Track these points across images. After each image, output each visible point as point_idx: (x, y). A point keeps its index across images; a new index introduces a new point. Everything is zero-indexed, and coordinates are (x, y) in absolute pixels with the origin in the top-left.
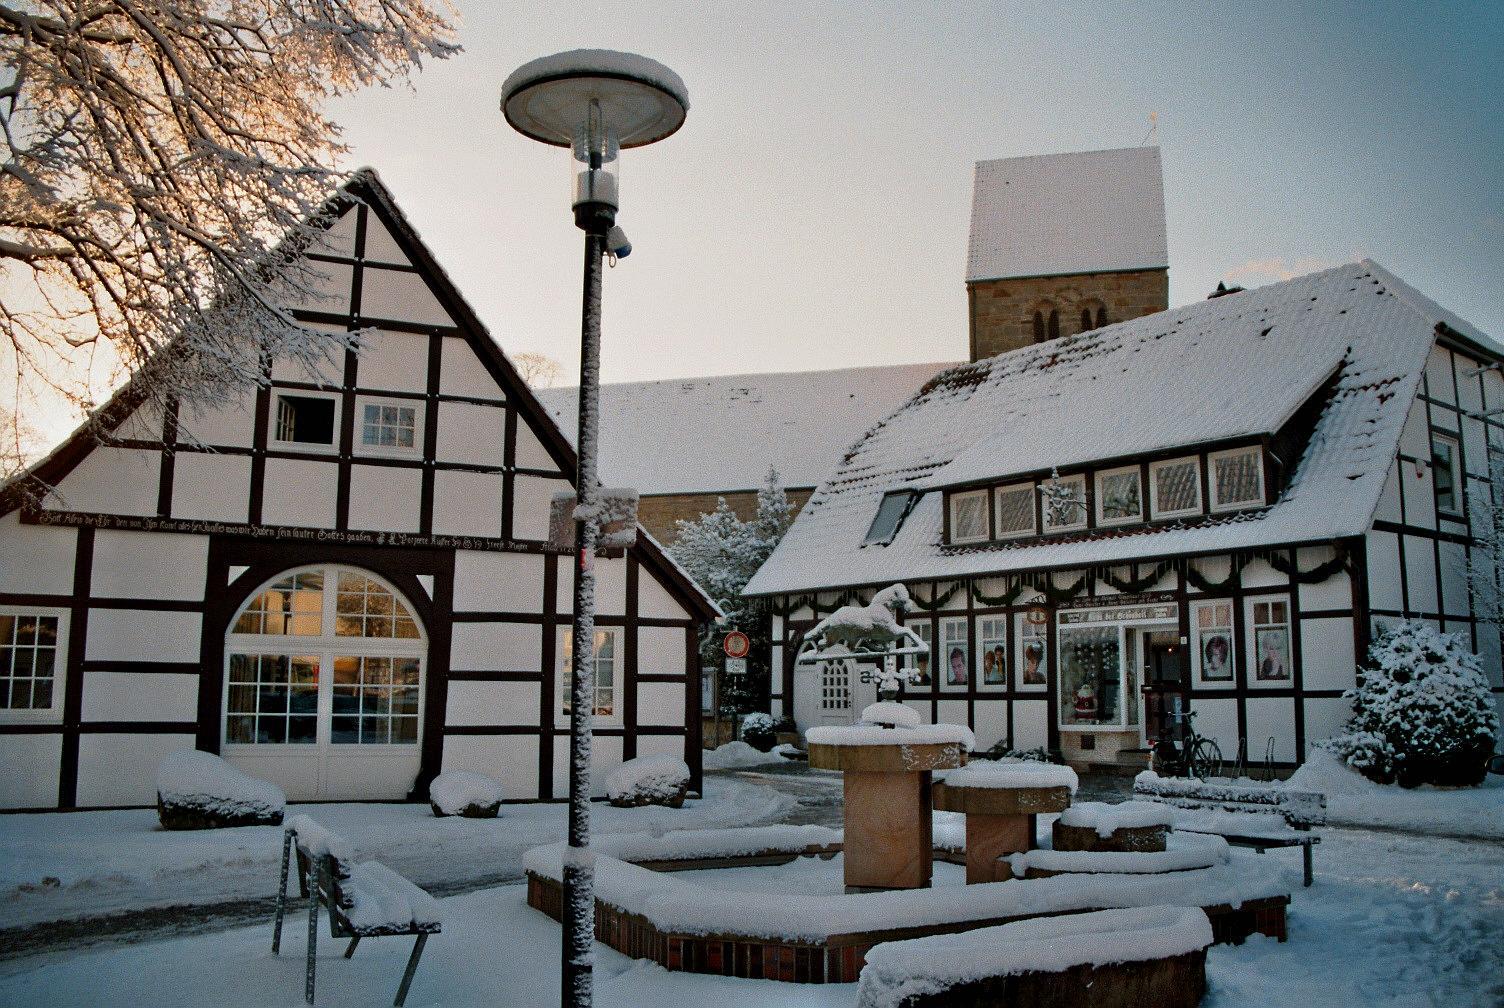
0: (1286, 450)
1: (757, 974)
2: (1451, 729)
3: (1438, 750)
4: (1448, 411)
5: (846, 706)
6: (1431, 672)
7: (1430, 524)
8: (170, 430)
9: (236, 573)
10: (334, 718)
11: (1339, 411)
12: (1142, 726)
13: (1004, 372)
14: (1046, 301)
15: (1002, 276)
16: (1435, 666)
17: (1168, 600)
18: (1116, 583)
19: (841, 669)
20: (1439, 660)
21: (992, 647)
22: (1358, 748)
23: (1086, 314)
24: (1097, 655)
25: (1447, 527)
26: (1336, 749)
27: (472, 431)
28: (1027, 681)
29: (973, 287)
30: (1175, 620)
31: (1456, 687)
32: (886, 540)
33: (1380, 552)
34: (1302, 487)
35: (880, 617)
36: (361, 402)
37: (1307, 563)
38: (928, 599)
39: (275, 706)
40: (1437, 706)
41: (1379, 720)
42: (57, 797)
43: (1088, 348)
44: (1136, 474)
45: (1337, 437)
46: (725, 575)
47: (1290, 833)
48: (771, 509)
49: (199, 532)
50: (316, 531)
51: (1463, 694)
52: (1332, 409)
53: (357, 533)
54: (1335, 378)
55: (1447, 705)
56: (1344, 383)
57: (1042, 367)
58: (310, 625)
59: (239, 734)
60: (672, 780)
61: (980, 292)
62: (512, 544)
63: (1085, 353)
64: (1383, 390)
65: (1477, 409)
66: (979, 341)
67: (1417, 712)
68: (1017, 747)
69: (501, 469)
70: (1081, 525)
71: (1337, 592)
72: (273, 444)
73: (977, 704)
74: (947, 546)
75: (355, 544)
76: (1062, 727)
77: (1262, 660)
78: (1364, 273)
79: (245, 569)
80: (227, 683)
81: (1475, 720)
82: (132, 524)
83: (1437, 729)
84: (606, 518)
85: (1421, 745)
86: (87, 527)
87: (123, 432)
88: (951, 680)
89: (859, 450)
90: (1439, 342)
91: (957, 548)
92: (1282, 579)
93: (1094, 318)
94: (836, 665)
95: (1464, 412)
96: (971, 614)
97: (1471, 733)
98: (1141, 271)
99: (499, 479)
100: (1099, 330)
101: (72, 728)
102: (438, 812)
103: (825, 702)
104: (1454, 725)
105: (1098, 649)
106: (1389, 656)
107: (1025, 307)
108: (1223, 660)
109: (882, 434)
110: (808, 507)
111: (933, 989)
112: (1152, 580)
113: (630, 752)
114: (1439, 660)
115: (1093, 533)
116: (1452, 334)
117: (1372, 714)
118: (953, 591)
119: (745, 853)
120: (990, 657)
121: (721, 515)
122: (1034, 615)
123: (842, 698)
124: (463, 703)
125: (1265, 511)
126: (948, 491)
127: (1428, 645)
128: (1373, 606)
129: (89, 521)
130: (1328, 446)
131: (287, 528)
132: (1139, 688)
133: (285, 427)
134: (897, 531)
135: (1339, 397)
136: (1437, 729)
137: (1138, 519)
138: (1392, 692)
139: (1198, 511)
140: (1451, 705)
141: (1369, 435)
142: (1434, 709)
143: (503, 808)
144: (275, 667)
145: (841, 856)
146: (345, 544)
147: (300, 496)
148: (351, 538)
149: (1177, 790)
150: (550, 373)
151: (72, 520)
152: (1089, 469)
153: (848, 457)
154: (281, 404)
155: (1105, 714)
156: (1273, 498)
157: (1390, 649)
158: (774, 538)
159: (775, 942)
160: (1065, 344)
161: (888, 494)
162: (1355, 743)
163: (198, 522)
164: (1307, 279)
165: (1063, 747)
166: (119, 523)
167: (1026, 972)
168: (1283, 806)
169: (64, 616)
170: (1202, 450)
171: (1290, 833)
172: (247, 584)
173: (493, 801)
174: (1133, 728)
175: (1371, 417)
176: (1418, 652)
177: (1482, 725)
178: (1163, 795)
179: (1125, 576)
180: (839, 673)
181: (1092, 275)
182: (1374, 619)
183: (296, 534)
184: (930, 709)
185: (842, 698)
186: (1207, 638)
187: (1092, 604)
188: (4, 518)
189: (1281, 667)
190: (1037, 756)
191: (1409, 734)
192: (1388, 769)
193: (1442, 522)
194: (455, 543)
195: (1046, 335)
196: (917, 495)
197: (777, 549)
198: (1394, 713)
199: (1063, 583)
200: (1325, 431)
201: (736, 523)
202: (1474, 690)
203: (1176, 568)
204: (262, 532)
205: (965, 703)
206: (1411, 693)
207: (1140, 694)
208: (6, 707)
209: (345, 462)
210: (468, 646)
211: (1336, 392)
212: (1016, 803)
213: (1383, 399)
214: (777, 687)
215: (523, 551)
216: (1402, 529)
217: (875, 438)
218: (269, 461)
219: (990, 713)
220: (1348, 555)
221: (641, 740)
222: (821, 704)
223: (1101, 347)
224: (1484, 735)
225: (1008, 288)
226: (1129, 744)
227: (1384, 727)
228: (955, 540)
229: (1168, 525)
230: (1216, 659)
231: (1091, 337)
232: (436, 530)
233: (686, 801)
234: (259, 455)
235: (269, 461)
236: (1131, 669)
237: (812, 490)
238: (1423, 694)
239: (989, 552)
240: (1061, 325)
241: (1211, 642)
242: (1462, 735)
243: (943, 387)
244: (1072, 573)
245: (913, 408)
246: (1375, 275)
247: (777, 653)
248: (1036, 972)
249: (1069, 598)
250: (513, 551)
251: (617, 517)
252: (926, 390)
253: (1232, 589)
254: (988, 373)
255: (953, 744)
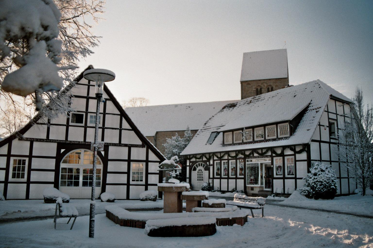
0: (295, 123)
1: (135, 227)
2: (325, 186)
3: (322, 191)
4: (334, 114)
5: (202, 180)
6: (322, 174)
7: (328, 140)
8: (49, 122)
9: (62, 150)
10: (83, 181)
11: (307, 115)
12: (264, 185)
13: (240, 105)
14: (259, 86)
15: (248, 80)
16: (323, 173)
17: (269, 157)
18: (258, 153)
19: (201, 172)
20: (324, 171)
21: (233, 167)
22: (304, 190)
23: (268, 89)
24: (254, 169)
25: (332, 141)
26: (300, 191)
27: (113, 121)
28: (240, 175)
29: (242, 83)
30: (270, 162)
31: (327, 177)
32: (211, 143)
33: (314, 147)
34: (297, 132)
35: (172, 162)
36: (89, 115)
37: (298, 149)
38: (219, 156)
39: (72, 179)
40: (322, 181)
41: (310, 185)
42: (25, 196)
43: (258, 99)
44: (251, 131)
45: (306, 121)
46: (176, 151)
47: (259, 207)
48: (187, 136)
49: (55, 142)
50: (79, 142)
51: (328, 179)
52: (306, 114)
53: (88, 142)
54: (308, 107)
55: (325, 181)
56: (309, 108)
57: (248, 103)
58: (84, 161)
59: (64, 184)
60: (153, 195)
61: (243, 84)
62: (121, 145)
63: (257, 100)
64: (317, 110)
65: (342, 113)
66: (243, 96)
67: (318, 183)
68: (238, 189)
69: (119, 129)
70: (251, 140)
71: (304, 156)
72: (70, 124)
73: (229, 180)
74: (224, 144)
75: (87, 145)
76: (247, 186)
77: (289, 171)
78: (317, 83)
79: (64, 150)
80: (60, 174)
81: (331, 184)
82: (41, 140)
83: (322, 186)
84: (99, 146)
85: (318, 190)
86: (32, 141)
87: (39, 121)
88: (224, 175)
89: (208, 122)
90: (331, 99)
91: (225, 145)
92: (292, 153)
93: (270, 90)
94: (200, 171)
95: (338, 115)
96: (228, 160)
97: (330, 187)
98: (281, 79)
99: (118, 131)
100: (261, 95)
101: (29, 182)
102: (102, 201)
103: (198, 179)
104: (326, 186)
105: (255, 168)
106: (313, 170)
107: (254, 87)
108: (280, 171)
109: (213, 118)
110: (196, 135)
111: (156, 228)
112: (265, 153)
113: (146, 189)
114: (324, 171)
115: (254, 142)
116: (334, 97)
117: (308, 183)
118: (224, 155)
119: (151, 208)
120: (232, 169)
121: (176, 137)
122: (240, 160)
123: (201, 178)
124: (110, 178)
125: (289, 137)
126: (224, 132)
127: (321, 168)
128: (312, 159)
129: (32, 140)
130: (304, 123)
131: (73, 141)
132: (264, 177)
133: (73, 120)
134: (214, 141)
135: (308, 111)
136: (322, 186)
137: (263, 139)
138: (313, 178)
139: (275, 137)
140: (325, 181)
141: (313, 120)
142: (322, 182)
143: (115, 201)
144: (71, 170)
145: (163, 210)
146: (85, 145)
147: (76, 134)
148: (87, 143)
149: (241, 198)
150: (146, 102)
151: (29, 139)
152: (253, 128)
153: (205, 124)
154: (72, 115)
155: (256, 183)
156: (291, 135)
157: (314, 168)
158: (188, 142)
159: (138, 221)
160: (253, 98)
161: (212, 132)
162: (303, 189)
163: (55, 140)
164: (305, 84)
165: (247, 190)
166: (38, 140)
167: (173, 226)
168: (258, 201)
169: (27, 159)
170: (277, 123)
171: (259, 207)
172: (65, 153)
173: (113, 199)
174: (262, 186)
175: (314, 116)
176: (319, 169)
177: (333, 186)
178: (239, 199)
179: (260, 151)
180: (201, 173)
181: (270, 79)
182: (312, 162)
183: (75, 143)
184: (219, 182)
185: (201, 178)
186: (277, 165)
187: (253, 158)
188: (1, 148)
189: (292, 172)
190: (241, 192)
191: (316, 187)
192: (311, 195)
193: (331, 140)
194: (109, 144)
195: (259, 94)
196: (218, 133)
197: (188, 145)
198: (313, 183)
199: (247, 153)
200: (304, 119)
201: (180, 139)
202: (331, 178)
203: (270, 150)
204: (68, 142)
205: (282, 180)
206: (316, 178)
207: (264, 178)
208: (20, 178)
209: (86, 127)
210: (111, 166)
211: (307, 110)
212: (194, 198)
213: (317, 112)
214: (188, 176)
215: (123, 146)
216: (320, 142)
217: (212, 119)
218: (106, 115)
219: (232, 182)
220: (306, 147)
221: (149, 187)
222: (197, 180)
223: (261, 99)
224: (333, 188)
225: (250, 83)
226: (261, 189)
227: (311, 186)
228: (225, 143)
229: (269, 140)
230: (279, 170)
231: (259, 97)
232: (87, 141)
233: (157, 200)
234: (68, 126)
235: (106, 115)
236: (262, 173)
237: (198, 130)
238: (319, 179)
239: (232, 146)
240: (262, 91)
241: (278, 167)
242: (328, 188)
243: (227, 108)
244: (249, 151)
245: (220, 113)
246: (319, 83)
247: (188, 168)
248: (176, 226)
249: (248, 156)
250: (121, 146)
251: (101, 146)
252: (223, 108)
253: (282, 155)
254: (236, 105)
255: (184, 187)
